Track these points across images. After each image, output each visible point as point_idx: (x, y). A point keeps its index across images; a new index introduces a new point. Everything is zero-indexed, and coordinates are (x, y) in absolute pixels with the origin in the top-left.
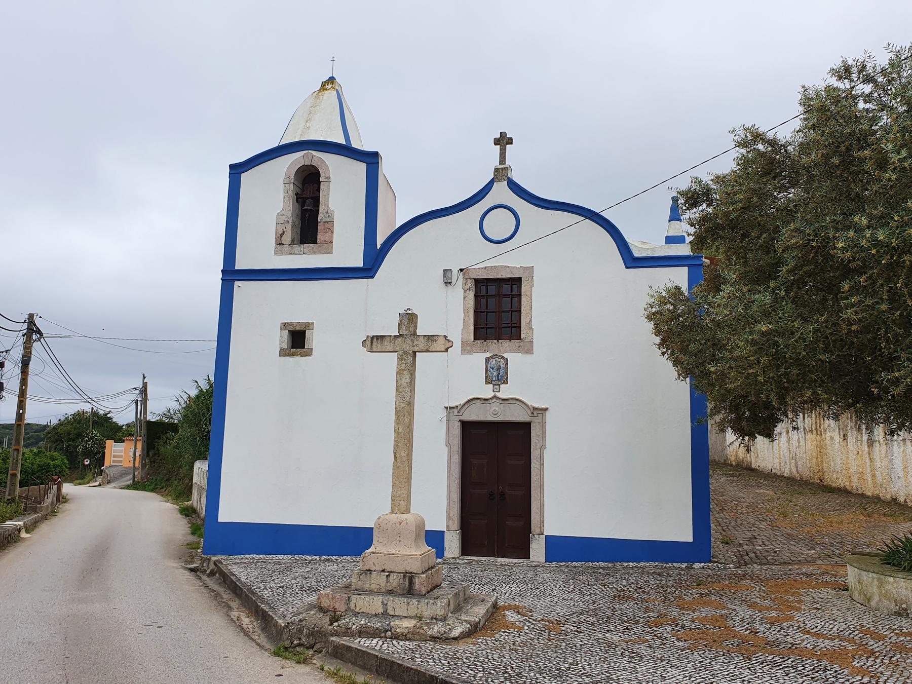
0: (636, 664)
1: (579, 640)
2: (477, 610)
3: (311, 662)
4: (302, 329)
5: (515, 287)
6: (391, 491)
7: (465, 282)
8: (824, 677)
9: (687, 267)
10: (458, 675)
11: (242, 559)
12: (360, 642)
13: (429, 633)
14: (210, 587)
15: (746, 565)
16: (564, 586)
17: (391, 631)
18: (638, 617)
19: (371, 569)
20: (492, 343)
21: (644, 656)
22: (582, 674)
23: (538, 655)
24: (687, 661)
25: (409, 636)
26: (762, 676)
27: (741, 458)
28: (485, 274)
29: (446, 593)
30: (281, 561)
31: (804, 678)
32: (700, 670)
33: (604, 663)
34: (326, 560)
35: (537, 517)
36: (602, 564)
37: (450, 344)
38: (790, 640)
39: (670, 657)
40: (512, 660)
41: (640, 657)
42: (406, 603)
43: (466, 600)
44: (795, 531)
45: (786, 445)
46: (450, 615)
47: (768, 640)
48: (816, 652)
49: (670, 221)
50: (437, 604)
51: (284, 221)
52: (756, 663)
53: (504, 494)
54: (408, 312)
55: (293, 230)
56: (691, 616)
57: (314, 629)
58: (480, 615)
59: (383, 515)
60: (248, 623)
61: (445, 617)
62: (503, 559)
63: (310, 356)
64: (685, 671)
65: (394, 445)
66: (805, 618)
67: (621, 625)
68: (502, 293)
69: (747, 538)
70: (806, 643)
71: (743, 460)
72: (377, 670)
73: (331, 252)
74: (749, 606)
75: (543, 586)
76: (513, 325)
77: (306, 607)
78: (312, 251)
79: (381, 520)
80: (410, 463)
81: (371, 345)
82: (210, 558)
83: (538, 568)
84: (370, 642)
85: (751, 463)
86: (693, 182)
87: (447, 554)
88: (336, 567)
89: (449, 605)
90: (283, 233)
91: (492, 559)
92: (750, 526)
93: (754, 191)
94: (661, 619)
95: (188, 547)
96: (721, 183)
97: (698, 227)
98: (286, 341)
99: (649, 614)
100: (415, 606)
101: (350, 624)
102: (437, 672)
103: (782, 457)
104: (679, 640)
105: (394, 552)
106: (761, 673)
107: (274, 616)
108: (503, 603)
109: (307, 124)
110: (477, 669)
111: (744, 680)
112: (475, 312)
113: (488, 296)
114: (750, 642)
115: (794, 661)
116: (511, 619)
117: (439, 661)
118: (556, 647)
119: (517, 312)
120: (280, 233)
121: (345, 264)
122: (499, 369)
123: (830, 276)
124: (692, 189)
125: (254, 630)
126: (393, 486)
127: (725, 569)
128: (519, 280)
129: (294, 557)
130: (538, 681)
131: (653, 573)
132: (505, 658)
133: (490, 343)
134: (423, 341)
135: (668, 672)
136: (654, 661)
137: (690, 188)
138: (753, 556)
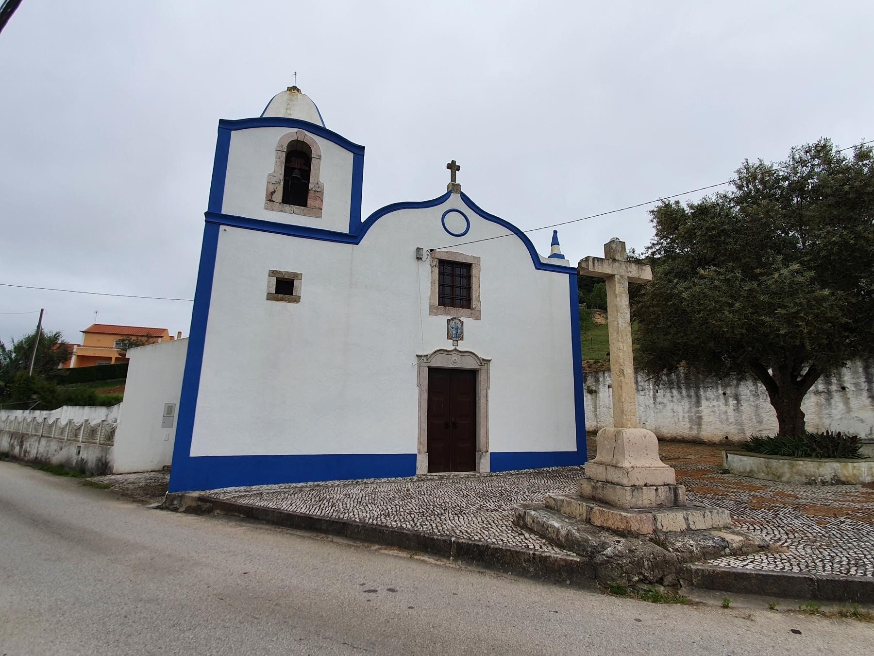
9: (568, 275)
19: (636, 484)
25: (744, 549)
63: (298, 302)
73: (320, 217)
81: (593, 265)
87: (419, 472)
90: (274, 192)
119: (469, 288)
122: (457, 329)
134: (635, 269)
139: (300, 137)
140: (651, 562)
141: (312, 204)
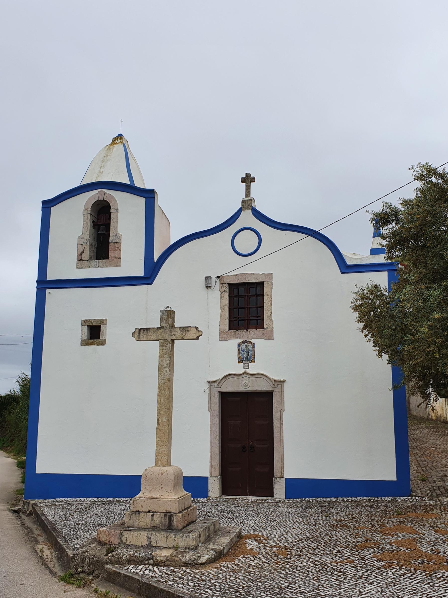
0: (341, 582)
1: (300, 563)
3: (91, 585)
4: (98, 324)
6: (155, 449)
7: (221, 285)
9: (387, 272)
10: (200, 594)
11: (54, 502)
12: (128, 568)
13: (183, 560)
14: (26, 525)
15: (437, 498)
17: (153, 559)
18: (349, 542)
19: (140, 510)
20: (242, 332)
21: (349, 574)
22: (297, 591)
23: (266, 576)
24: (381, 578)
25: (167, 563)
26: (438, 589)
27: (439, 414)
29: (199, 526)
30: (83, 503)
32: (390, 585)
33: (316, 581)
35: (279, 464)
36: (328, 499)
37: (200, 333)
39: (369, 575)
40: (245, 581)
41: (346, 575)
42: (166, 537)
43: (215, 532)
46: (201, 545)
49: (373, 237)
50: (189, 537)
51: (84, 242)
53: (253, 447)
54: (168, 309)
56: (390, 540)
57: (93, 558)
58: (224, 544)
59: (149, 468)
60: (49, 554)
61: (196, 547)
62: (254, 497)
64: (379, 587)
65: (157, 413)
67: (334, 549)
68: (249, 294)
69: (440, 476)
71: (441, 416)
73: (119, 266)
74: (436, 531)
75: (280, 519)
76: (259, 318)
77: (90, 541)
78: (104, 265)
79: (147, 472)
81: (139, 336)
82: (29, 502)
84: (135, 569)
86: (385, 206)
87: (211, 495)
89: (199, 537)
90: (83, 252)
91: (245, 497)
93: (429, 213)
96: (408, 206)
97: (389, 240)
98: (86, 334)
99: (358, 539)
101: (122, 554)
102: (183, 593)
104: (378, 560)
105: (158, 496)
107: (66, 548)
108: (246, 533)
109: (101, 169)
111: (424, 594)
112: (230, 309)
114: (433, 561)
116: (250, 547)
118: (281, 569)
120: (81, 252)
124: (384, 211)
126: (156, 445)
127: (421, 501)
128: (262, 284)
129: (94, 500)
131: (366, 505)
132: (239, 579)
133: (241, 332)
134: (179, 332)
135: (365, 588)
136: (356, 579)
137: (382, 211)
139: (100, 196)
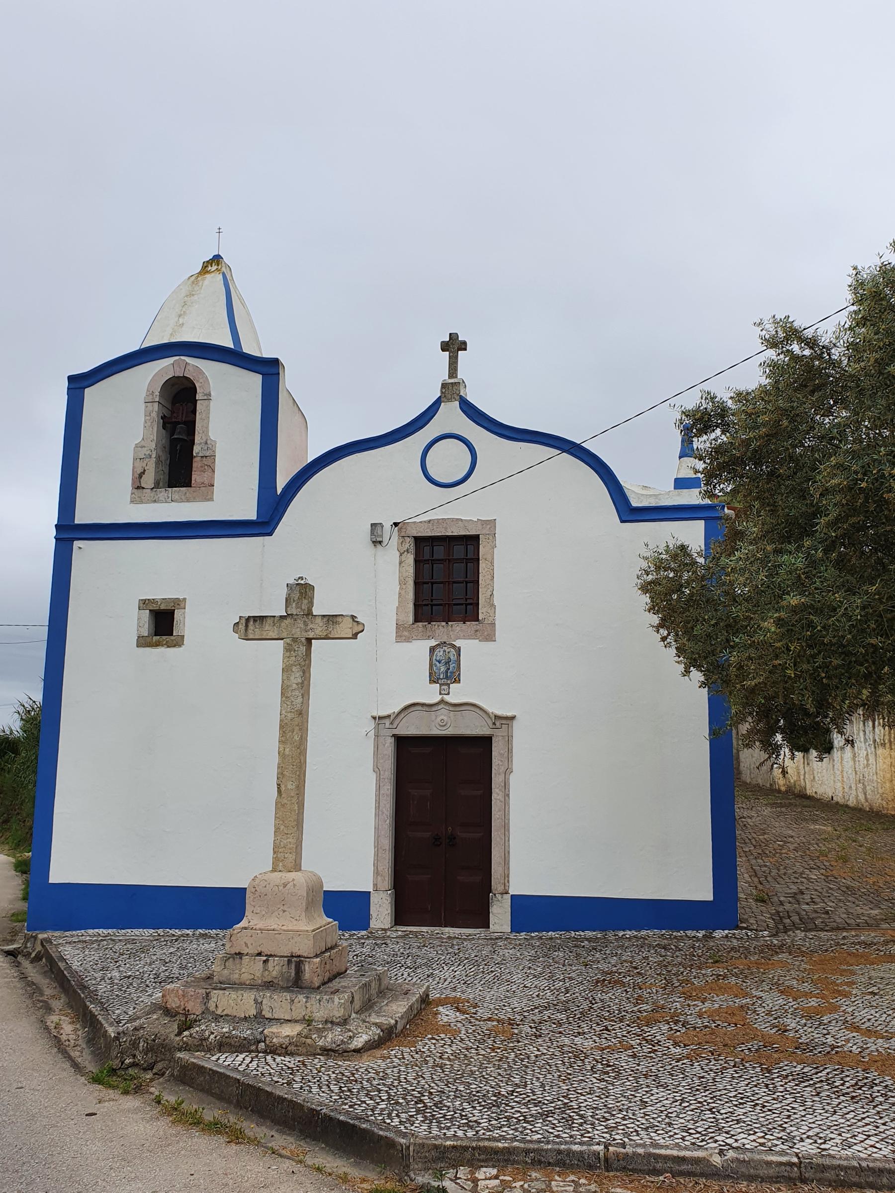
1: (535, 1049)
2: (394, 1008)
4: (169, 608)
5: (471, 548)
8: (869, 1096)
9: (703, 521)
10: (351, 1107)
11: (82, 935)
13: (320, 1043)
14: (29, 979)
15: (785, 932)
16: (530, 968)
17: (264, 1042)
22: (529, 1101)
23: (472, 1072)
24: (682, 1076)
25: (291, 1048)
26: (782, 1096)
27: (792, 781)
28: (428, 530)
29: (351, 983)
30: (136, 938)
31: (842, 1098)
32: (697, 1090)
33: (564, 1083)
34: (201, 935)
36: (589, 934)
37: (357, 628)
38: (830, 1040)
39: (659, 1071)
40: (433, 1082)
44: (857, 883)
45: (851, 763)
46: (354, 1015)
47: (800, 1041)
48: (863, 1057)
49: (680, 458)
52: (778, 1077)
53: (455, 838)
54: (300, 581)
55: (157, 467)
56: (699, 1008)
57: (154, 1041)
58: (397, 1015)
63: (180, 646)
64: (677, 1092)
65: (278, 774)
66: (855, 1008)
67: (598, 1025)
69: (791, 893)
70: (851, 1045)
72: (238, 1101)
73: (211, 499)
76: (435, 602)
78: (183, 497)
79: (257, 881)
80: (300, 799)
82: (36, 935)
83: (499, 941)
85: (805, 789)
87: (374, 924)
88: (213, 945)
89: (352, 1002)
90: (143, 473)
91: (437, 930)
92: (797, 876)
93: (784, 412)
94: (655, 1015)
95: (13, 918)
98: (147, 626)
99: (641, 1006)
100: (301, 1005)
101: (207, 1033)
103: (845, 780)
104: (676, 1044)
105: (275, 927)
106: (782, 1092)
107: (103, 1022)
108: (438, 995)
110: (380, 1097)
111: (757, 1104)
113: (434, 560)
114: (774, 1046)
115: (830, 1072)
116: (445, 1019)
117: (327, 1085)
118: (500, 1060)
120: (139, 472)
121: (232, 516)
122: (448, 663)
123: (886, 531)
124: (702, 408)
125: (77, 1043)
128: (475, 539)
129: (157, 932)
130: (464, 1114)
131: (656, 945)
132: (424, 1078)
133: (436, 626)
134: (321, 624)
135: (652, 1095)
138: (795, 918)
140: (148, 1043)
141: (199, 480)
